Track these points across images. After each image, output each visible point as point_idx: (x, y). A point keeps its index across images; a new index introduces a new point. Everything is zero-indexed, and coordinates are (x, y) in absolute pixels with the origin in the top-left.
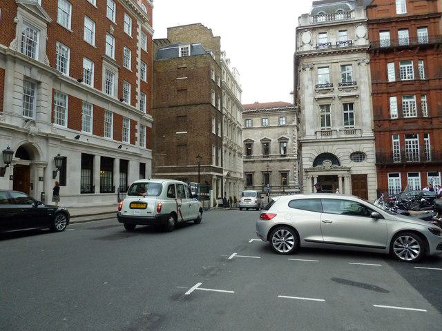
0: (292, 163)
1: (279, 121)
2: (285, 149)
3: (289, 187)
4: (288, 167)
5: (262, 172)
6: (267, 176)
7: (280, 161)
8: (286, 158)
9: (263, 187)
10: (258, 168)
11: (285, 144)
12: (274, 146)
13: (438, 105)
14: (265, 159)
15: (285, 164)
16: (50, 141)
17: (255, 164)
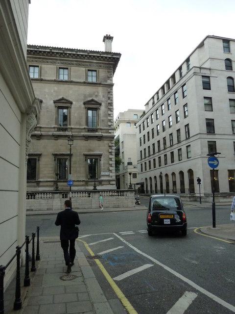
0: (106, 142)
1: (87, 76)
2: (65, 118)
3: (101, 183)
4: (99, 148)
5: (55, 155)
6: (62, 162)
7: (87, 138)
8: (67, 133)
9: (55, 182)
10: (47, 148)
11: (65, 111)
12: (77, 112)
13: (64, 113)
14: (62, 133)
15: (94, 144)
16: (37, 196)
17: (43, 142)
